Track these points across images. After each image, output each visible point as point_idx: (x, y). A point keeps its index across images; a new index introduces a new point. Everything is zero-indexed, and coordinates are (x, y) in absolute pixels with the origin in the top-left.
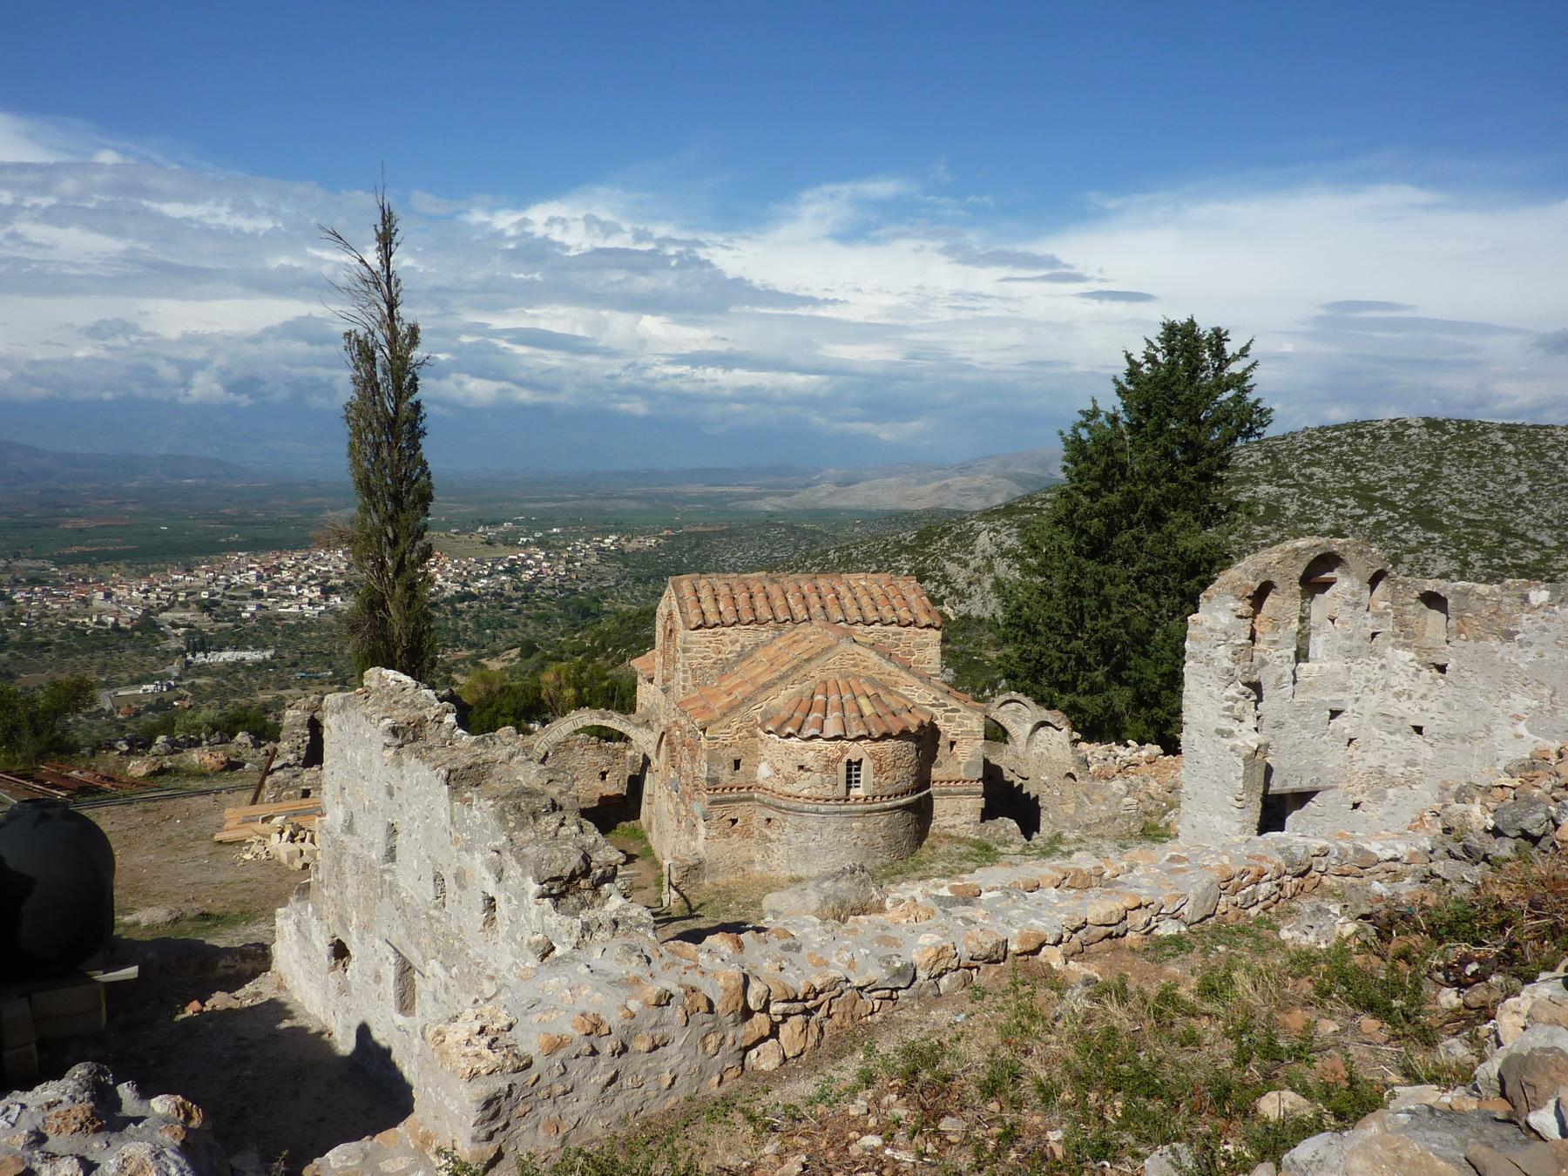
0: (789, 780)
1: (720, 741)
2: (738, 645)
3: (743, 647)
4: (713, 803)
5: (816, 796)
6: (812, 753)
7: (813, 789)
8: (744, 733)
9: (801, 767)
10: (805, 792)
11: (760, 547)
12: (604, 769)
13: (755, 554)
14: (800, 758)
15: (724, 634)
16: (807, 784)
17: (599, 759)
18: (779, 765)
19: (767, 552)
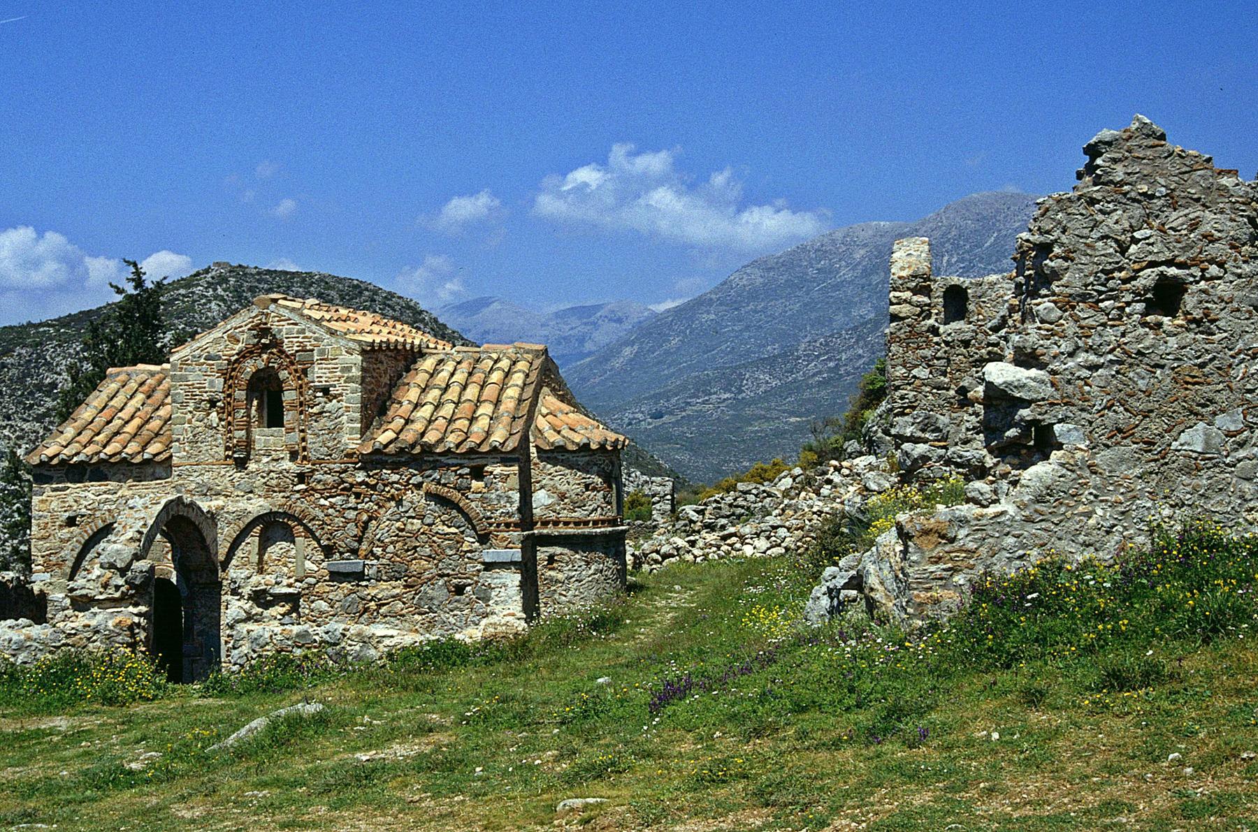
0: (577, 505)
18: (564, 488)
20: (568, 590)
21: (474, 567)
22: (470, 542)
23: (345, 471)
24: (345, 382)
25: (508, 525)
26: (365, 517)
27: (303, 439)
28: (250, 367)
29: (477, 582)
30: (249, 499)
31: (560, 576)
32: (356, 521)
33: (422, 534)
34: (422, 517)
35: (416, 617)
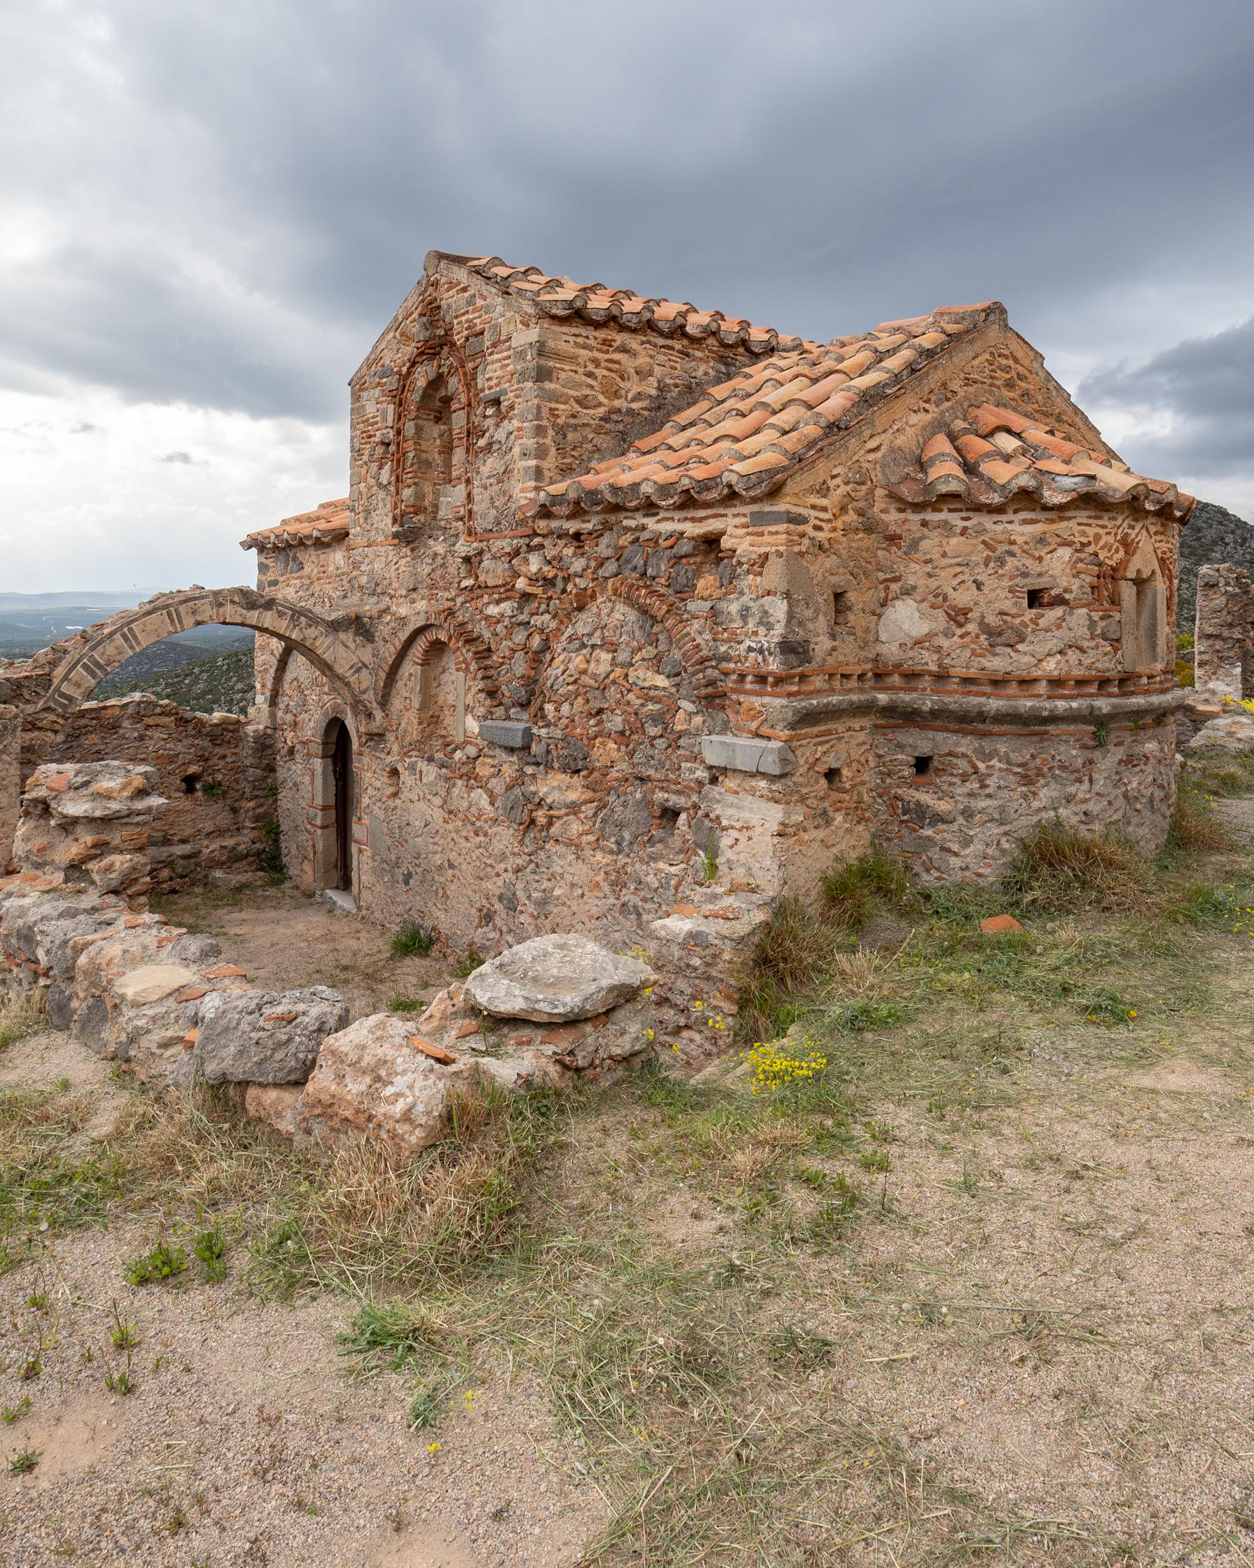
1: (808, 529)
2: (653, 381)
3: (662, 388)
4: (807, 718)
5: (1078, 672)
6: (1065, 553)
7: (1073, 656)
8: (851, 517)
9: (1035, 598)
10: (1051, 666)
11: (139, 663)
12: (193, 769)
13: (134, 670)
14: (1034, 567)
15: (624, 349)
16: (1053, 644)
17: (179, 748)
18: (963, 598)
19: (146, 667)
20: (967, 842)
21: (692, 771)
22: (687, 714)
23: (517, 552)
24: (519, 382)
25: (761, 679)
26: (536, 642)
27: (469, 496)
28: (421, 379)
29: (696, 807)
30: (413, 602)
31: (943, 806)
32: (525, 648)
33: (614, 682)
34: (613, 648)
35: (599, 855)
